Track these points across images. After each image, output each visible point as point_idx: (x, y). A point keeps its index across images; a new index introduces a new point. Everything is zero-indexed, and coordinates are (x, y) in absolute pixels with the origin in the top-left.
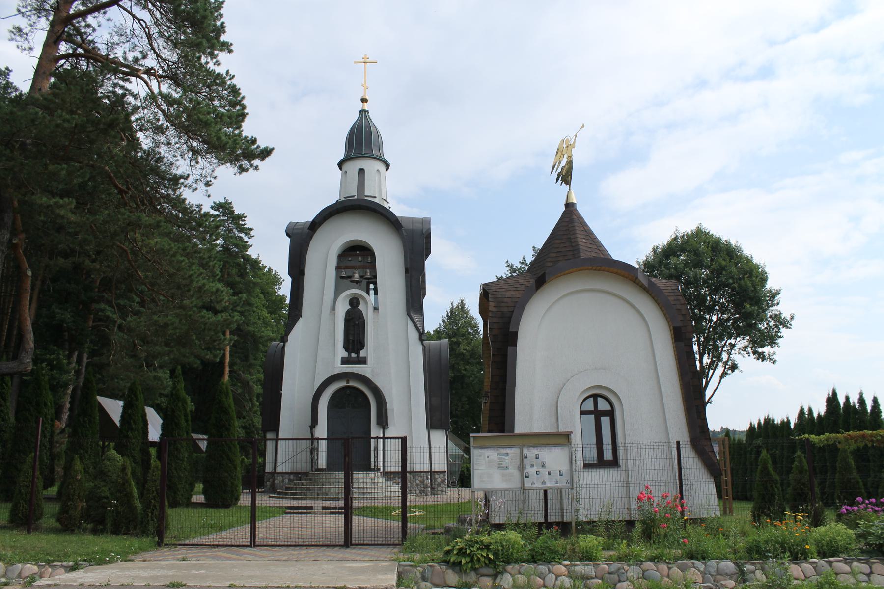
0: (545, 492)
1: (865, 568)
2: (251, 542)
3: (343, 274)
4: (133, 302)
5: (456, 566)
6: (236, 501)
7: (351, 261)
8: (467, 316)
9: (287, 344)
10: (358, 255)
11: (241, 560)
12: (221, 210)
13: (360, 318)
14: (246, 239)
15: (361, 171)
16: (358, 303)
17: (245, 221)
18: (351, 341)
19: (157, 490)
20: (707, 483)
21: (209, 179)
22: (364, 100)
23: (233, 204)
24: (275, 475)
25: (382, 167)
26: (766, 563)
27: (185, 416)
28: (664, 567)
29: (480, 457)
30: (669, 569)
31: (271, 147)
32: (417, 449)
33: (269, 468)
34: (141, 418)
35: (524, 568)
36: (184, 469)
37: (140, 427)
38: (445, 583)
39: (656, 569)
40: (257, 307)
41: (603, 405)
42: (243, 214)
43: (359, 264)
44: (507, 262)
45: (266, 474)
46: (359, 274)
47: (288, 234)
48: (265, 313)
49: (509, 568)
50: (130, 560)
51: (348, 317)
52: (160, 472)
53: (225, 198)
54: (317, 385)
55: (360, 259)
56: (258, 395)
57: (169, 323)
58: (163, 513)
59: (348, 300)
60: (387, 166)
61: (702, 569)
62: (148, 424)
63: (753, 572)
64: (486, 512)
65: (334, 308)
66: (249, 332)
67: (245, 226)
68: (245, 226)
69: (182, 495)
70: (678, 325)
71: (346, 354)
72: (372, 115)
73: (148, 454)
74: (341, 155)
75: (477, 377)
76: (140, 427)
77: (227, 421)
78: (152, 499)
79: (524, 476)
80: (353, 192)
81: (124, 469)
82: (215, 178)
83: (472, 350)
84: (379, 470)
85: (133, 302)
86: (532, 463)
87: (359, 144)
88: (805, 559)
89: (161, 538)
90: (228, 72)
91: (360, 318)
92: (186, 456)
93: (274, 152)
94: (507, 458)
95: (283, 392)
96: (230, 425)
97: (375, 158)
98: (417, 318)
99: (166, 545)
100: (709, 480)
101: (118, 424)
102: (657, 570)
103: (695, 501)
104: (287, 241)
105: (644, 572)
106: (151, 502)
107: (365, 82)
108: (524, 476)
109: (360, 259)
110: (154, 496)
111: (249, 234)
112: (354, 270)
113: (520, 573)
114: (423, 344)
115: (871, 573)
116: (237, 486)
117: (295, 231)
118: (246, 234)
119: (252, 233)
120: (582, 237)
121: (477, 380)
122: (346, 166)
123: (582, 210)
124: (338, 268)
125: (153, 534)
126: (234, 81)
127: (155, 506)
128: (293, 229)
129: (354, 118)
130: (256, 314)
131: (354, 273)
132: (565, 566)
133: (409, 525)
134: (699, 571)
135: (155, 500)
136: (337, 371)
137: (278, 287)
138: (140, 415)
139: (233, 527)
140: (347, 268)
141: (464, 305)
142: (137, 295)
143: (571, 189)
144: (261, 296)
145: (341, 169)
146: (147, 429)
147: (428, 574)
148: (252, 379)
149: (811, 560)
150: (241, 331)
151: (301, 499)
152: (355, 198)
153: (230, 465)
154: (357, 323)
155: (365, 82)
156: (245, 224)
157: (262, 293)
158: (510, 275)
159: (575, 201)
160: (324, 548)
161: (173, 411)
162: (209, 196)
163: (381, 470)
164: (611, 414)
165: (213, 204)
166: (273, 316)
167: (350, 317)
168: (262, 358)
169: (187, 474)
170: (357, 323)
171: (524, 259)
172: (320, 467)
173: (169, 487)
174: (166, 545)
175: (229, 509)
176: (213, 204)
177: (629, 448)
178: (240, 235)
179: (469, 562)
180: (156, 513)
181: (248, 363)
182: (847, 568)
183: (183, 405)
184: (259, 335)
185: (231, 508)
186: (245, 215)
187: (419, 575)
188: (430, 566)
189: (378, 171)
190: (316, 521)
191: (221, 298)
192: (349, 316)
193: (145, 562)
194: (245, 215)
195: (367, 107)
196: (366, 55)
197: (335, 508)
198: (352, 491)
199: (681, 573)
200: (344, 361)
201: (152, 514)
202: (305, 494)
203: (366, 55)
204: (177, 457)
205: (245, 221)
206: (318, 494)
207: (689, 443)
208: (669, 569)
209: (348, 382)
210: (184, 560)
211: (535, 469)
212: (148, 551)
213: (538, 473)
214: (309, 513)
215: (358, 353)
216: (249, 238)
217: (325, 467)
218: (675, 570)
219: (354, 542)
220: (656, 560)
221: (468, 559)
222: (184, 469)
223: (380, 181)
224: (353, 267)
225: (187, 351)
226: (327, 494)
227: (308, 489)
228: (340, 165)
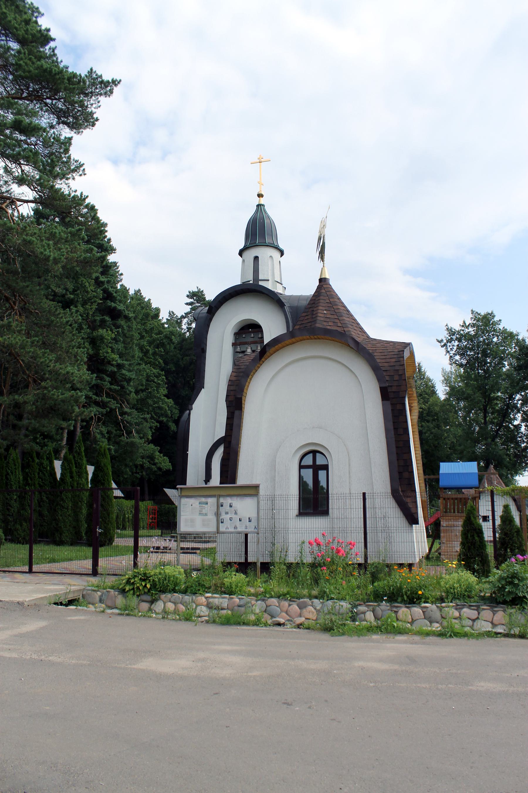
0: (246, 536)
1: (473, 614)
3: (238, 349)
4: (105, 381)
5: (123, 591)
8: (424, 378)
9: (192, 412)
10: (250, 332)
12: (195, 298)
15: (256, 258)
20: (405, 531)
23: (205, 292)
25: (276, 254)
26: (379, 605)
28: (286, 604)
29: (186, 505)
30: (290, 605)
35: (174, 597)
38: (115, 605)
39: (278, 605)
41: (320, 461)
43: (252, 340)
49: (163, 596)
51: (232, 388)
53: (197, 288)
55: (252, 335)
60: (282, 253)
61: (318, 608)
63: (364, 613)
64: (152, 549)
70: (384, 385)
74: (242, 245)
75: (431, 433)
79: (220, 521)
80: (250, 278)
83: (429, 408)
85: (105, 381)
86: (227, 511)
88: (419, 603)
94: (206, 506)
95: (189, 452)
96: (104, 480)
97: (267, 246)
100: (407, 528)
102: (279, 606)
103: (393, 548)
105: (267, 606)
107: (260, 179)
108: (220, 521)
109: (252, 335)
112: (247, 346)
113: (170, 601)
115: (478, 618)
117: (200, 315)
120: (324, 309)
121: (432, 435)
123: (336, 285)
124: (234, 345)
131: (247, 348)
132: (206, 598)
134: (315, 609)
142: (108, 376)
143: (325, 265)
147: (104, 597)
149: (423, 605)
152: (251, 282)
155: (260, 179)
158: (449, 338)
159: (327, 277)
160: (78, 576)
164: (325, 467)
165: (188, 294)
176: (188, 294)
177: (335, 498)
179: (132, 589)
182: (456, 614)
187: (98, 599)
188: (107, 591)
189: (271, 256)
195: (262, 201)
197: (188, 549)
199: (299, 610)
203: (260, 156)
207: (391, 497)
208: (290, 605)
211: (229, 516)
213: (231, 519)
218: (295, 607)
220: (281, 598)
221: (131, 587)
228: (241, 253)
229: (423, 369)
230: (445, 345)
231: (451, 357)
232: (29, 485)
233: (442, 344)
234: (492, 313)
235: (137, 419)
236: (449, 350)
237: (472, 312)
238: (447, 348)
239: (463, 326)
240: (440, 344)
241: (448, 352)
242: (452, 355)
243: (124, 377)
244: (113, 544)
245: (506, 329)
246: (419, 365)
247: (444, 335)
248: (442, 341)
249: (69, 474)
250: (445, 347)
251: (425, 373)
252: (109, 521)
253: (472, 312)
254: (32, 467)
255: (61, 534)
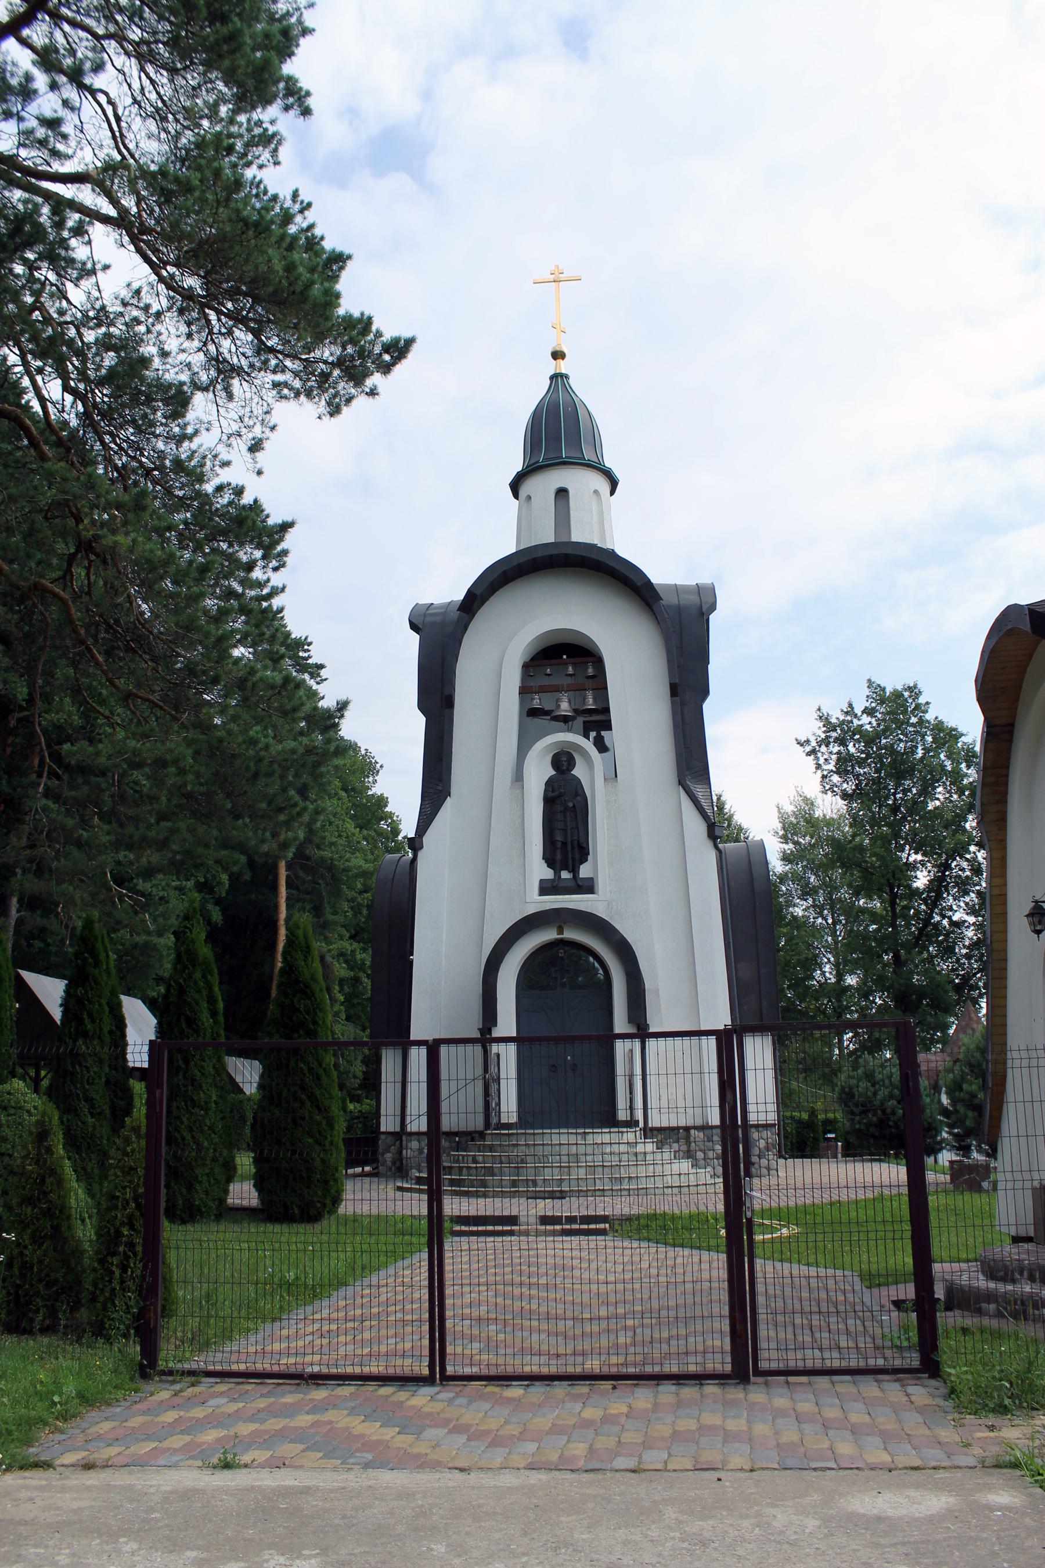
2: (432, 1366)
3: (536, 703)
6: (334, 1205)
7: (550, 676)
8: (729, 825)
9: (421, 854)
11: (422, 1463)
13: (576, 795)
14: (312, 683)
15: (562, 493)
16: (571, 763)
17: (309, 651)
18: (559, 845)
19: (135, 1199)
21: (257, 431)
22: (557, 355)
24: (404, 1138)
27: (208, 1002)
31: (406, 334)
32: (1024, 1054)
33: (388, 1123)
34: (107, 1009)
36: (210, 1128)
37: (106, 1030)
40: (335, 815)
42: (306, 638)
44: (819, 709)
45: (383, 1137)
46: (570, 702)
47: (414, 627)
48: (350, 826)
50: (37, 1465)
51: (550, 795)
52: (143, 1143)
54: (491, 939)
55: (570, 670)
56: (342, 982)
57: (168, 757)
58: (155, 1273)
59: (549, 758)
62: (125, 1026)
65: (518, 777)
66: (323, 860)
67: (310, 661)
68: (310, 661)
69: (207, 1192)
71: (548, 874)
72: (576, 384)
73: (128, 1095)
74: (518, 466)
76: (106, 1030)
77: (308, 1013)
78: (123, 1224)
81: (42, 1135)
82: (273, 428)
84: (637, 1123)
87: (554, 439)
89: (150, 1352)
90: (295, 195)
91: (576, 795)
92: (214, 1098)
93: (415, 349)
95: (416, 958)
96: (315, 1023)
98: (699, 791)
99: (163, 1373)
101: (59, 1023)
104: (414, 639)
106: (118, 1233)
110: (131, 1217)
111: (319, 675)
114: (716, 847)
116: (337, 1169)
117: (429, 619)
118: (313, 676)
119: (323, 673)
122: (528, 487)
124: (525, 691)
125: (125, 1336)
126: (311, 216)
127: (131, 1245)
128: (425, 615)
129: (537, 390)
130: (333, 828)
131: (558, 701)
133: (765, 1269)
135: (132, 1227)
136: (531, 910)
137: (371, 779)
138: (104, 1002)
139: (343, 1283)
140: (542, 690)
141: (723, 804)
144: (343, 794)
145: (516, 495)
146: (124, 1035)
148: (329, 951)
150: (308, 858)
151: (476, 1195)
153: (318, 1118)
154: (571, 805)
156: (309, 657)
157: (343, 789)
158: (823, 736)
161: (182, 991)
162: (259, 473)
163: (641, 1124)
166: (365, 832)
167: (556, 794)
168: (346, 912)
169: (216, 1140)
170: (571, 805)
171: (850, 705)
172: (504, 1120)
173: (174, 1173)
174: (163, 1373)
175: (317, 1227)
178: (301, 676)
180: (136, 1267)
181: (322, 920)
183: (204, 976)
184: (341, 865)
185: (325, 1222)
186: (309, 640)
189: (596, 492)
190: (551, 1261)
191: (295, 702)
192: (553, 791)
193: (91, 1473)
194: (309, 640)
195: (563, 366)
196: (557, 266)
197: (571, 1220)
198: (751, 1197)
200: (547, 888)
201: (124, 1268)
202: (484, 1184)
204: (192, 1100)
205: (309, 651)
206: (514, 1183)
209: (560, 931)
210: (227, 1466)
212: (108, 1404)
214: (511, 1233)
215: (575, 871)
216: (318, 683)
217: (514, 1119)
219: (763, 1365)
222: (210, 1128)
223: (601, 512)
224: (556, 689)
225: (215, 832)
226: (535, 1183)
227: (490, 1171)
228: (515, 486)
229: (727, 807)
230: (813, 752)
231: (824, 777)
232: (85, 1035)
233: (808, 749)
234: (915, 686)
235: (163, 889)
236: (822, 761)
237: (870, 682)
238: (817, 758)
239: (847, 713)
240: (801, 749)
241: (818, 767)
242: (825, 773)
243: (138, 788)
244: (341, 1210)
245: (941, 722)
246: (719, 799)
247: (815, 730)
248: (808, 742)
249: (205, 1005)
250: (812, 757)
251: (731, 816)
252: (332, 1143)
253: (870, 682)
254: (96, 982)
255: (190, 1187)
